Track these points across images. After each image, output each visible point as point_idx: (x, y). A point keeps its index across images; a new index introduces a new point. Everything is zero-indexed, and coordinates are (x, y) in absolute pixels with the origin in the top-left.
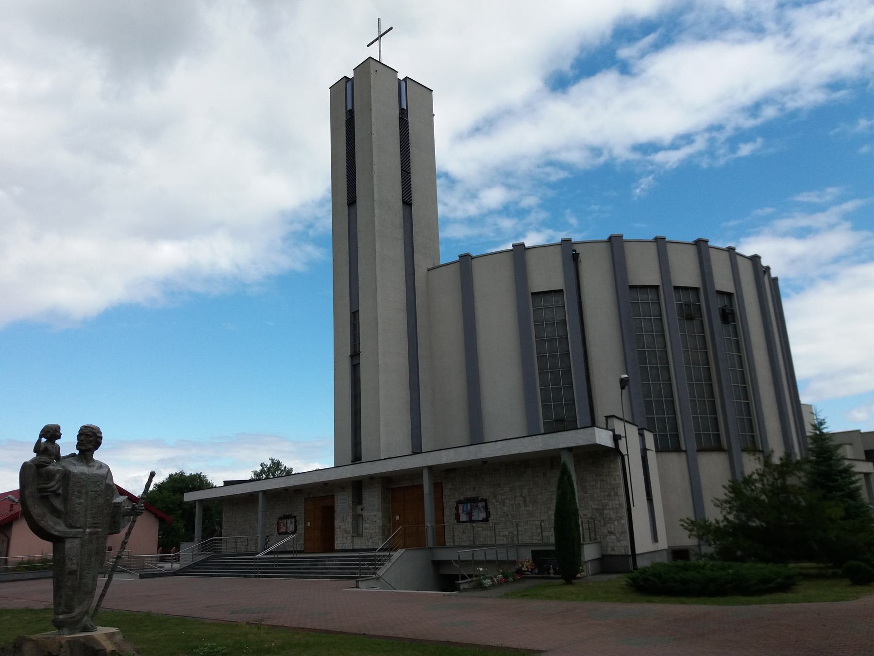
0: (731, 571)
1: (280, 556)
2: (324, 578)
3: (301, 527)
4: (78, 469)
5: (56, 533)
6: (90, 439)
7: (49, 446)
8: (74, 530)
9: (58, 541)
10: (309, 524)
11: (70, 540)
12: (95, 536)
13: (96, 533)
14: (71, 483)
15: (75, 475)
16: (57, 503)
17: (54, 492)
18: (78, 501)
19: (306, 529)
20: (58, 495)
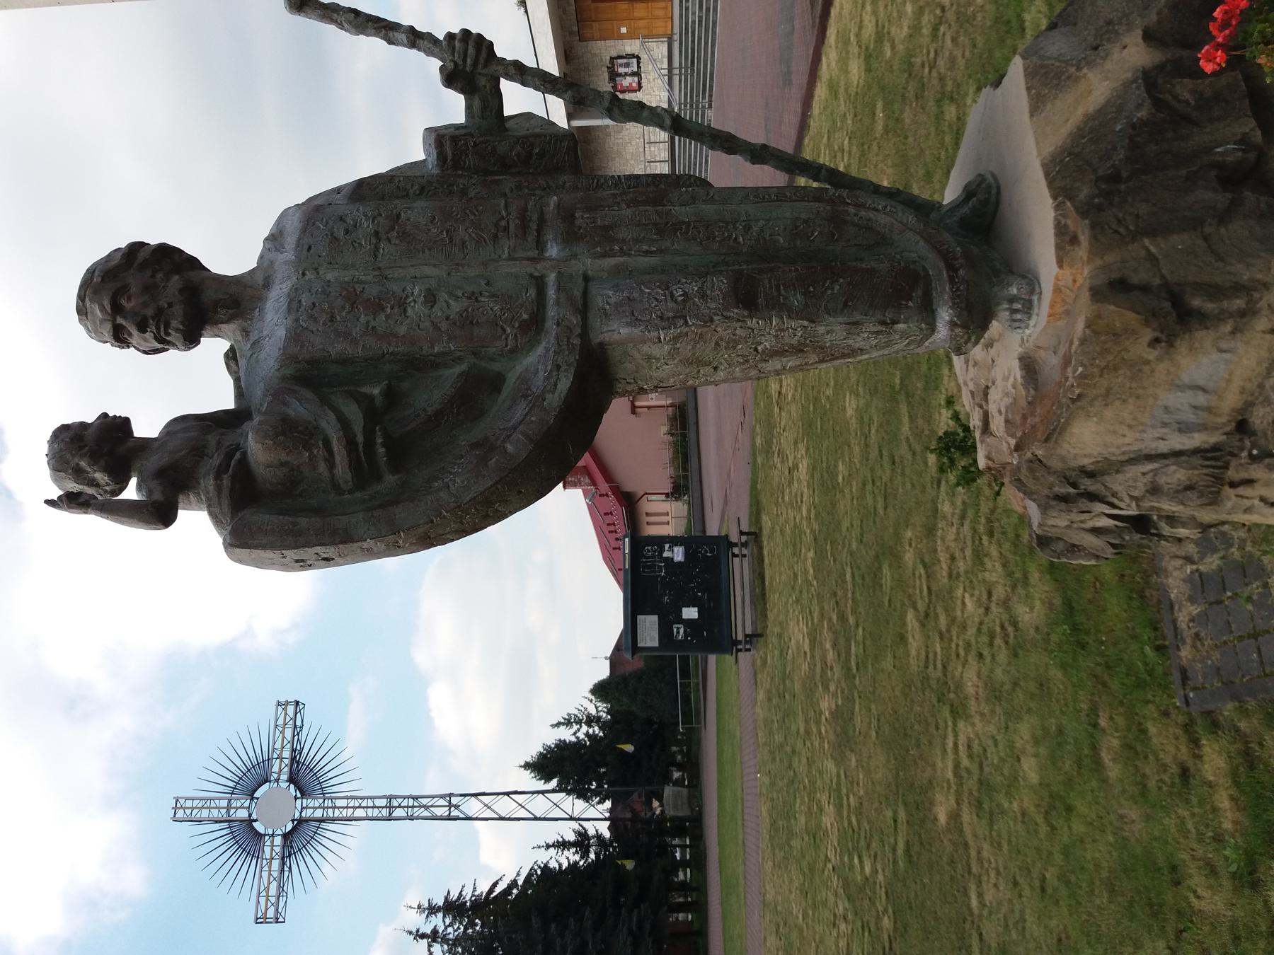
0: (758, 429)
1: (676, 64)
2: (711, 87)
3: (631, 46)
4: (274, 322)
5: (565, 384)
6: (144, 293)
7: (154, 462)
8: (552, 312)
9: (836, 461)
10: (624, 30)
11: (595, 321)
12: (582, 219)
13: (567, 216)
14: (339, 348)
15: (295, 336)
16: (430, 396)
17: (373, 415)
18: (417, 309)
19: (631, 36)
20: (392, 395)
